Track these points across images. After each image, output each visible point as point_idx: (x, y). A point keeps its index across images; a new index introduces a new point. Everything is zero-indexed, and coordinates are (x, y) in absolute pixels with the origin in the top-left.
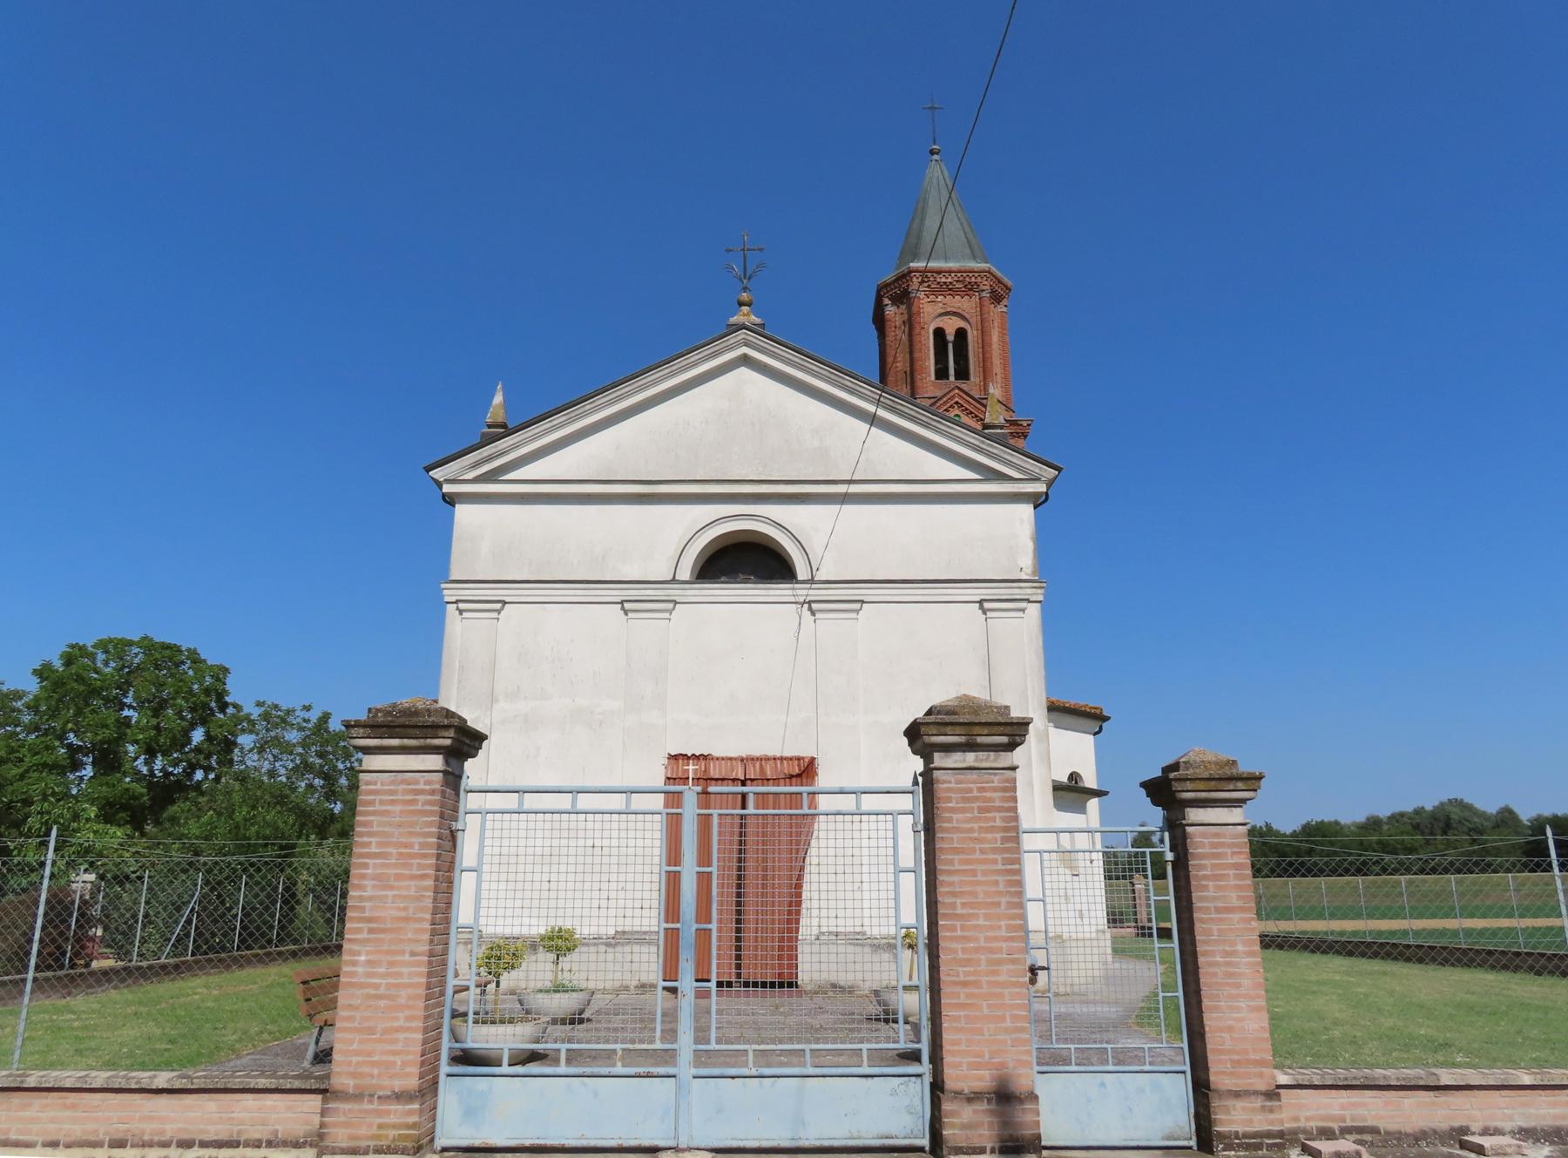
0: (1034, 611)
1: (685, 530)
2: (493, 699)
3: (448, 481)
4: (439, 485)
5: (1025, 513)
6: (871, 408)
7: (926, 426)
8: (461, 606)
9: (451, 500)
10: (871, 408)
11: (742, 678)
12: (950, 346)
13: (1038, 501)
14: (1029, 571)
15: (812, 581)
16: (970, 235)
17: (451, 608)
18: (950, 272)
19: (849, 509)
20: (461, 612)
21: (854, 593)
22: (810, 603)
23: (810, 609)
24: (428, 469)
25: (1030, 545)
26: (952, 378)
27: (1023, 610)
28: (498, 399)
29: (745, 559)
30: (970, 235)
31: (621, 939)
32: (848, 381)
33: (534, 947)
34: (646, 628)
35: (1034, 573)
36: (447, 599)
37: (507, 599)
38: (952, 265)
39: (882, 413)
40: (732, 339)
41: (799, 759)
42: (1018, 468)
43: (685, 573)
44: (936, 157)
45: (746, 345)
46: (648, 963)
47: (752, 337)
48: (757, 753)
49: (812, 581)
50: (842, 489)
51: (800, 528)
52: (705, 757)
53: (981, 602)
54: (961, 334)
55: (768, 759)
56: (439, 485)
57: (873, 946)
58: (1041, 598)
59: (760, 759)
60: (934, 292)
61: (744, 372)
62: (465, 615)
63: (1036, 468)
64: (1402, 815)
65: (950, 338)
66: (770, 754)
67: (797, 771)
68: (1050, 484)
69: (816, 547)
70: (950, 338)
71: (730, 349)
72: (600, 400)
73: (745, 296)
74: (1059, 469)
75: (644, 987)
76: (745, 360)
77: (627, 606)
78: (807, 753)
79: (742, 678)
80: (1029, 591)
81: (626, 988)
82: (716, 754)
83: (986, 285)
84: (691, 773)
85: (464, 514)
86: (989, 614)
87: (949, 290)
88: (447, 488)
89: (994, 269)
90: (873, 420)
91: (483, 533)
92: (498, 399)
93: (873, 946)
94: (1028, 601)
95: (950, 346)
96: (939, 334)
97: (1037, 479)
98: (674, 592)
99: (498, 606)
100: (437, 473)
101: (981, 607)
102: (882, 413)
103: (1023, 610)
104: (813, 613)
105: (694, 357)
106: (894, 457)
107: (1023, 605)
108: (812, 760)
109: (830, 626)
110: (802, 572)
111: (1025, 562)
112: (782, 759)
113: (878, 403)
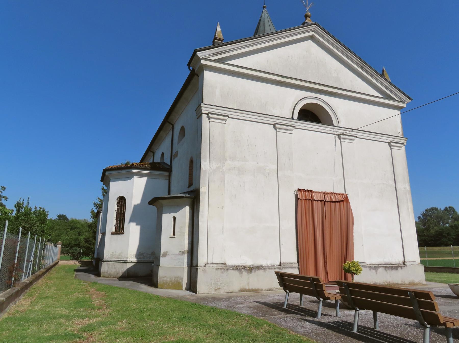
0: (403, 148)
1: (289, 101)
7: (372, 76)
11: (315, 159)
14: (401, 134)
17: (204, 116)
28: (219, 29)
29: (311, 114)
32: (349, 54)
35: (402, 135)
36: (203, 111)
42: (398, 97)
43: (296, 117)
45: (314, 31)
47: (318, 29)
49: (338, 126)
51: (338, 108)
61: (310, 42)
64: (436, 209)
71: (309, 31)
76: (312, 38)
79: (315, 159)
80: (403, 141)
84: (305, 201)
88: (202, 62)
92: (219, 29)
101: (389, 145)
103: (226, 120)
107: (226, 118)
111: (399, 130)
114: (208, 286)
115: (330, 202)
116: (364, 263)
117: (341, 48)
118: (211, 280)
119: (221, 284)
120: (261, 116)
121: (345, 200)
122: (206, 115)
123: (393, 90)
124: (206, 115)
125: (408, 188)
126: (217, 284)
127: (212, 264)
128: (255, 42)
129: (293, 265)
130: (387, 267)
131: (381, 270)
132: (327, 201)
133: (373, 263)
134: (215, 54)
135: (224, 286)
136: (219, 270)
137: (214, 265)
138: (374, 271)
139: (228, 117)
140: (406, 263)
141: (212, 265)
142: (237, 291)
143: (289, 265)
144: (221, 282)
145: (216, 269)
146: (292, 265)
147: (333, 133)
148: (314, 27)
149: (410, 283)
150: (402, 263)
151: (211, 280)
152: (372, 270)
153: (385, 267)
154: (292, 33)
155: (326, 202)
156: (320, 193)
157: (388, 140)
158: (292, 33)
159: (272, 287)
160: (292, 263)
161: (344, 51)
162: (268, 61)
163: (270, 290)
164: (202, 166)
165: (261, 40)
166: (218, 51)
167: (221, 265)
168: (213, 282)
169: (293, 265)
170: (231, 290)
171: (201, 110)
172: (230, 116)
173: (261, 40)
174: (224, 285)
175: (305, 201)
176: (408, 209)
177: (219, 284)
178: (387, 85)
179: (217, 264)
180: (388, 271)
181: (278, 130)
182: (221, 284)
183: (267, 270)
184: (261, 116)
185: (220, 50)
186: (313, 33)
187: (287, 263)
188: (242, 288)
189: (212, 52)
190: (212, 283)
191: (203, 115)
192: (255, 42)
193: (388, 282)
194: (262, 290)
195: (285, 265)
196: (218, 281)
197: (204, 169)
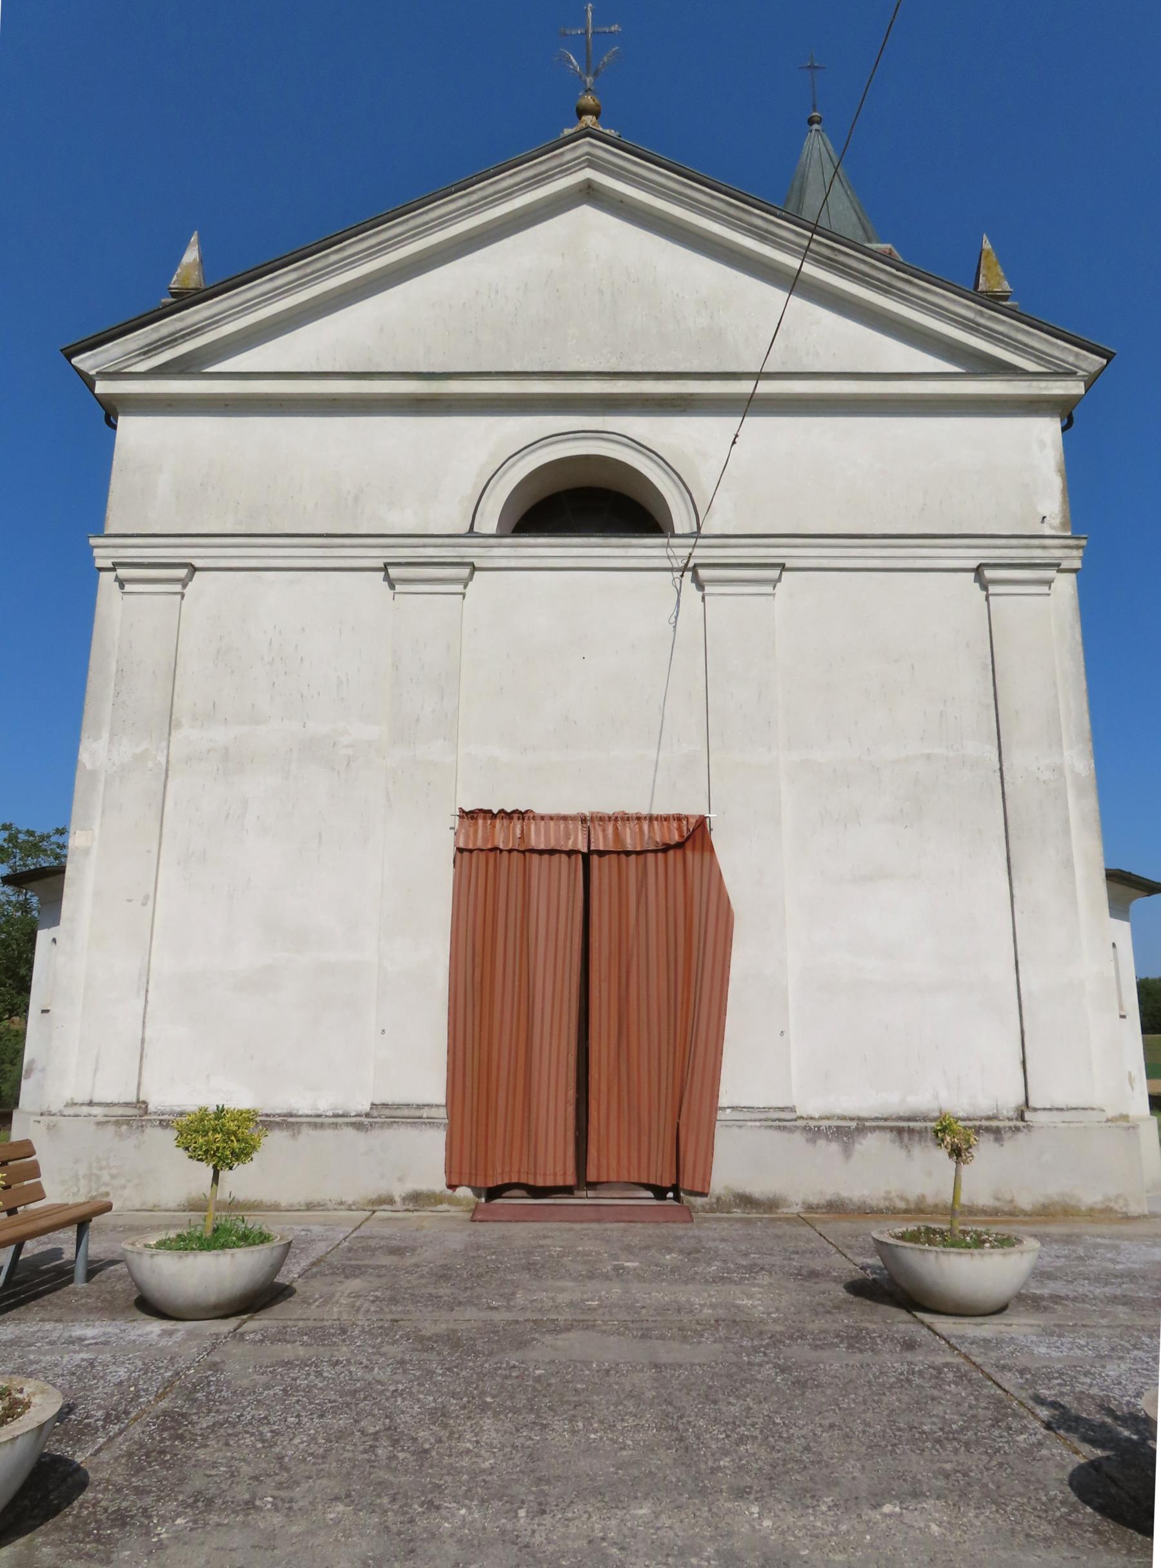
0: (1065, 585)
1: (491, 455)
2: (171, 723)
4: (88, 381)
5: (1049, 428)
6: (793, 262)
7: (885, 289)
8: (122, 573)
9: (111, 411)
10: (793, 262)
13: (1067, 412)
14: (1057, 521)
15: (697, 535)
16: (860, 214)
17: (106, 578)
19: (756, 425)
20: (122, 583)
21: (765, 559)
22: (694, 569)
23: (696, 579)
24: (70, 353)
25: (1056, 483)
27: (1049, 583)
28: (191, 255)
29: (587, 504)
30: (860, 214)
31: (385, 1116)
33: (164, 1124)
34: (425, 610)
35: (1064, 525)
36: (99, 563)
37: (198, 563)
39: (809, 269)
40: (568, 153)
41: (679, 818)
43: (489, 523)
44: (816, 126)
46: (423, 1158)
47: (602, 151)
48: (609, 809)
49: (697, 535)
50: (745, 387)
51: (675, 451)
52: (522, 815)
53: (978, 571)
55: (626, 818)
56: (88, 381)
57: (806, 1129)
58: (1077, 564)
59: (615, 819)
61: (587, 214)
62: (128, 587)
63: (1067, 353)
66: (631, 810)
67: (676, 838)
68: (1091, 382)
69: (703, 480)
71: (565, 170)
73: (589, 100)
74: (1108, 356)
75: (417, 1199)
76: (589, 194)
77: (394, 572)
78: (693, 807)
79: (580, 693)
80: (1058, 553)
81: (390, 1201)
82: (539, 810)
84: (496, 856)
85: (129, 427)
86: (992, 589)
88: (101, 387)
90: (794, 284)
91: (160, 463)
92: (191, 255)
93: (806, 1129)
94: (1057, 567)
97: (1069, 374)
99: (182, 573)
100: (86, 362)
102: (809, 269)
104: (700, 586)
106: (829, 341)
108: (702, 822)
109: (728, 606)
110: (681, 521)
111: (1049, 503)
112: (651, 818)
113: (805, 254)
114: (63, 1182)
115: (618, 853)
116: (782, 1109)
117: (719, 201)
118: (76, 1161)
119: (113, 1177)
120: (327, 546)
121: (695, 836)
122: (972, 575)
123: (1000, 328)
124: (972, 575)
125: (1077, 761)
126: (98, 1178)
127: (91, 1104)
128: (309, 270)
129: (425, 1113)
130: (911, 1131)
131: (871, 1144)
132: (601, 853)
133: (838, 1111)
134: (149, 350)
135: (124, 1187)
136: (111, 1129)
137: (96, 1110)
138: (834, 1147)
139: (783, 567)
140: (1027, 1116)
141: (85, 1110)
142: (172, 1204)
143: (406, 1112)
144: (114, 1171)
145: (99, 1124)
146: (417, 1113)
147: (666, 563)
148: (586, 149)
149: (1044, 1207)
150: (1012, 1114)
151: (76, 1161)
152: (822, 1143)
153: (900, 1131)
154: (475, 197)
155: (595, 859)
156: (565, 818)
157: (971, 556)
158: (475, 197)
159: (316, 1197)
160: (419, 1107)
161: (732, 211)
162: (382, 329)
163: (310, 1207)
164: (84, 757)
165: (333, 258)
166: (155, 336)
167: (120, 1111)
168: (82, 1170)
169: (425, 1113)
170: (151, 1201)
171: (94, 559)
172: (789, 563)
173: (333, 258)
174: (122, 1181)
175: (496, 856)
176: (1068, 864)
177: (106, 1178)
178: (970, 315)
179: (107, 1105)
180: (917, 1150)
181: (708, 589)
182: (113, 1177)
183: (305, 1130)
184: (327, 546)
185: (164, 331)
186: (589, 173)
187: (399, 1106)
188: (194, 1194)
189: (133, 346)
190: (81, 1173)
191: (102, 574)
192: (309, 270)
193: (1008, 1197)
194: (275, 1207)
195: (387, 1112)
196: (101, 1168)
197: (89, 767)
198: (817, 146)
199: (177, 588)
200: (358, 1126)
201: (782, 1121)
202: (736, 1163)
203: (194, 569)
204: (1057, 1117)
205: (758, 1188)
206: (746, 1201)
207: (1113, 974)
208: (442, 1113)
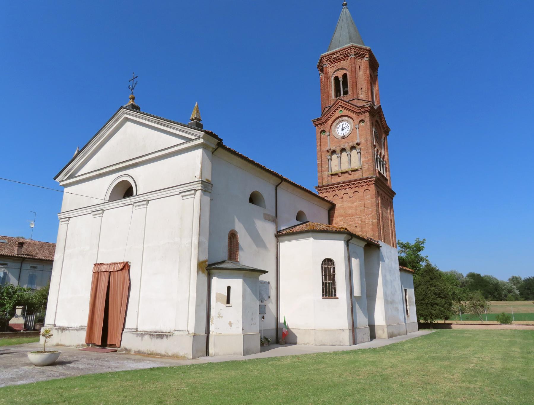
1: (107, 184)
3: (61, 181)
12: (341, 83)
13: (202, 146)
18: (337, 52)
26: (342, 95)
29: (126, 191)
38: (337, 49)
40: (120, 113)
54: (345, 76)
60: (333, 63)
61: (128, 123)
65: (341, 79)
70: (341, 79)
71: (121, 116)
72: (90, 145)
76: (127, 119)
82: (105, 263)
83: (352, 52)
87: (338, 60)
89: (355, 44)
95: (341, 83)
96: (336, 79)
98: (104, 207)
100: (58, 180)
105: (111, 123)
130: (153, 335)
131: (147, 337)
134: (66, 175)
138: (140, 338)
153: (151, 335)
180: (153, 339)
186: (126, 116)
198: (345, 12)
199: (193, 196)
200: (77, 330)
201: (137, 332)
202: (128, 341)
203: (149, 201)
204: (179, 332)
205: (128, 347)
206: (126, 349)
207: (226, 294)
208: (86, 328)
